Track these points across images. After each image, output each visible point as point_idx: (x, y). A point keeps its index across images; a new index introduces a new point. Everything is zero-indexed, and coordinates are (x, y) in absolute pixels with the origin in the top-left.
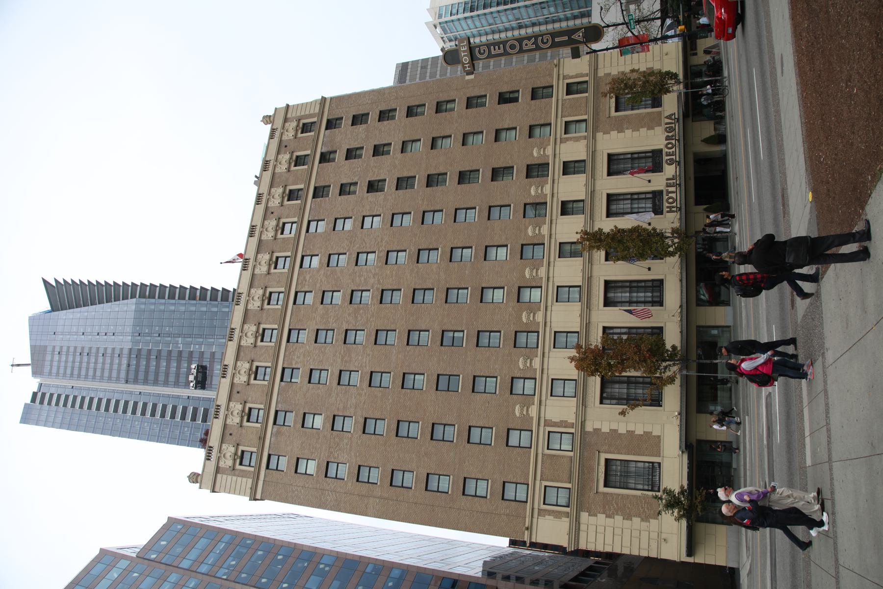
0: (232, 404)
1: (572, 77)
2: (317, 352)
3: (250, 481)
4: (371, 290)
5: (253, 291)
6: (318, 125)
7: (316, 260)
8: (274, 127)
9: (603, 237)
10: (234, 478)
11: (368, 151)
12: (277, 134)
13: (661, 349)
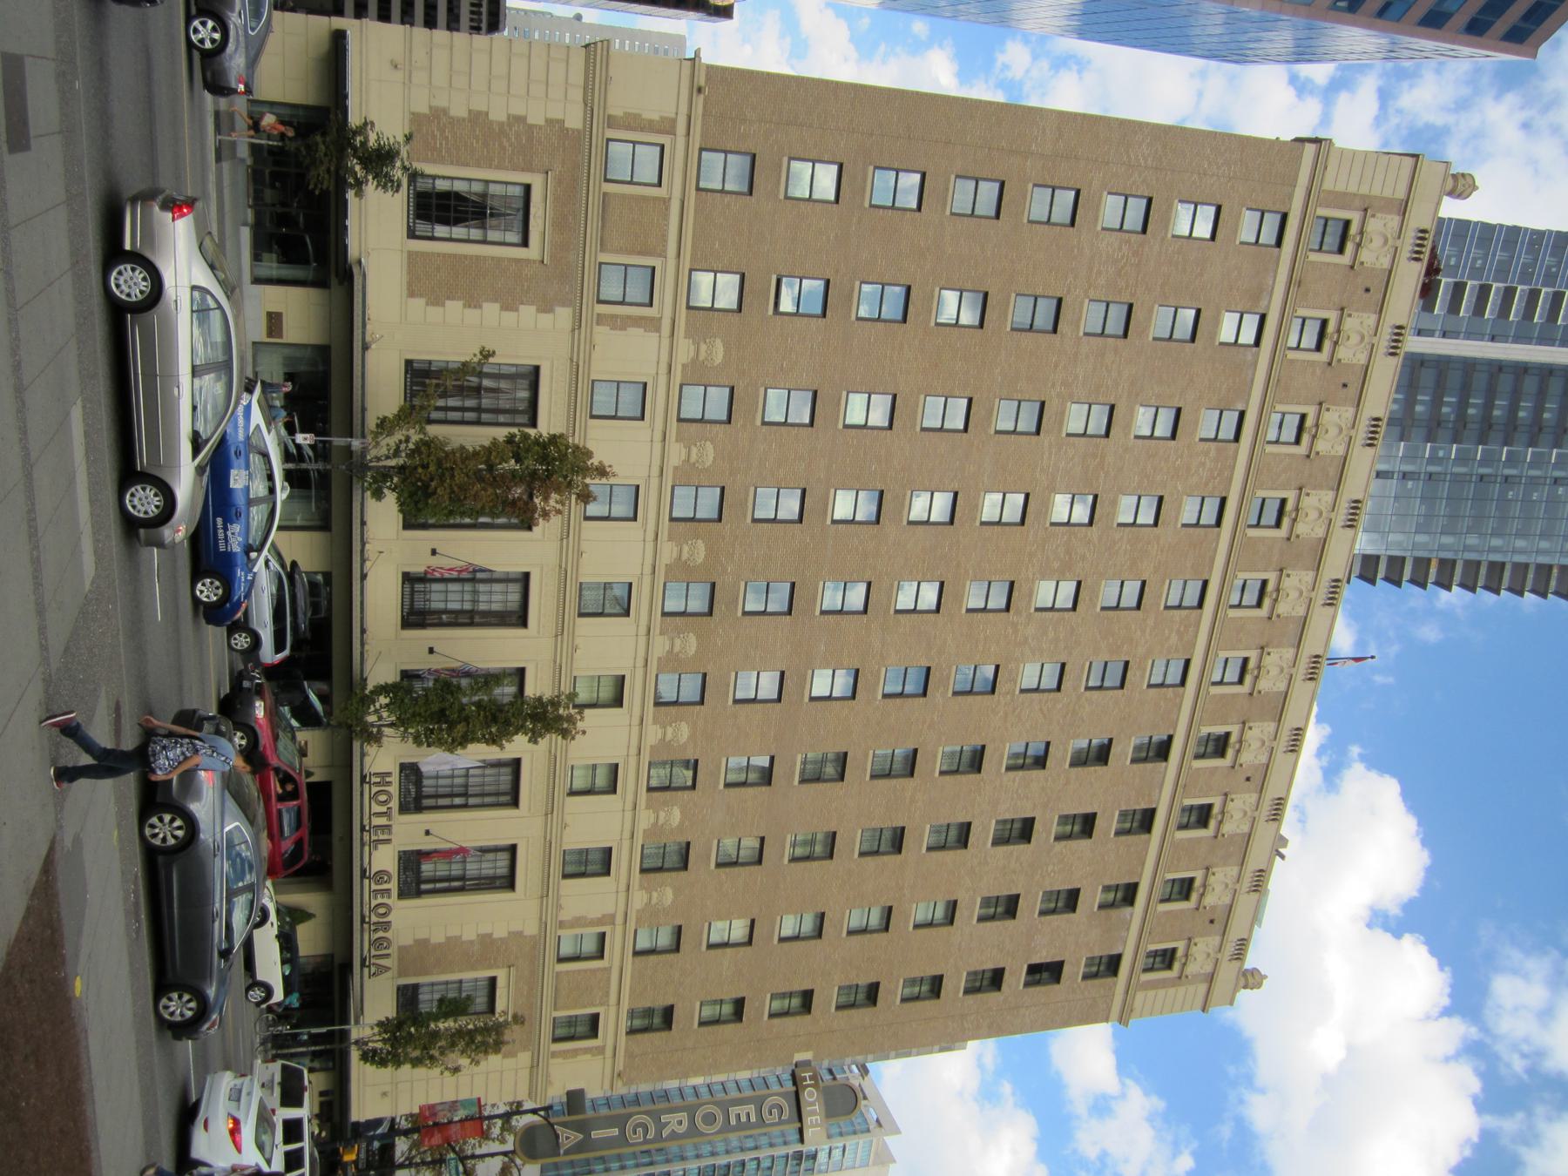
0: (1385, 263)
1: (586, 1051)
2: (1159, 478)
3: (1328, 185)
4: (1032, 610)
5: (1301, 611)
6: (1156, 895)
7: (1189, 515)
8: (1236, 964)
9: (529, 725)
10: (1364, 190)
11: (1029, 907)
12: (1230, 948)
13: (406, 495)
